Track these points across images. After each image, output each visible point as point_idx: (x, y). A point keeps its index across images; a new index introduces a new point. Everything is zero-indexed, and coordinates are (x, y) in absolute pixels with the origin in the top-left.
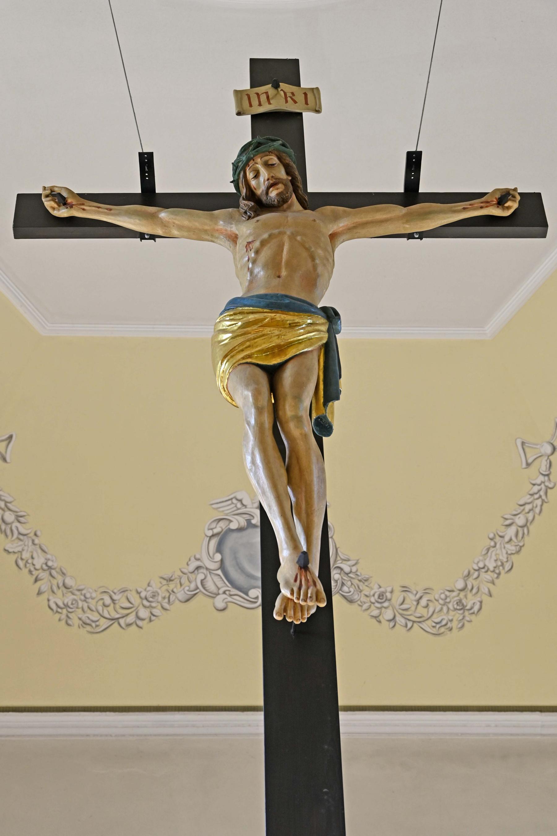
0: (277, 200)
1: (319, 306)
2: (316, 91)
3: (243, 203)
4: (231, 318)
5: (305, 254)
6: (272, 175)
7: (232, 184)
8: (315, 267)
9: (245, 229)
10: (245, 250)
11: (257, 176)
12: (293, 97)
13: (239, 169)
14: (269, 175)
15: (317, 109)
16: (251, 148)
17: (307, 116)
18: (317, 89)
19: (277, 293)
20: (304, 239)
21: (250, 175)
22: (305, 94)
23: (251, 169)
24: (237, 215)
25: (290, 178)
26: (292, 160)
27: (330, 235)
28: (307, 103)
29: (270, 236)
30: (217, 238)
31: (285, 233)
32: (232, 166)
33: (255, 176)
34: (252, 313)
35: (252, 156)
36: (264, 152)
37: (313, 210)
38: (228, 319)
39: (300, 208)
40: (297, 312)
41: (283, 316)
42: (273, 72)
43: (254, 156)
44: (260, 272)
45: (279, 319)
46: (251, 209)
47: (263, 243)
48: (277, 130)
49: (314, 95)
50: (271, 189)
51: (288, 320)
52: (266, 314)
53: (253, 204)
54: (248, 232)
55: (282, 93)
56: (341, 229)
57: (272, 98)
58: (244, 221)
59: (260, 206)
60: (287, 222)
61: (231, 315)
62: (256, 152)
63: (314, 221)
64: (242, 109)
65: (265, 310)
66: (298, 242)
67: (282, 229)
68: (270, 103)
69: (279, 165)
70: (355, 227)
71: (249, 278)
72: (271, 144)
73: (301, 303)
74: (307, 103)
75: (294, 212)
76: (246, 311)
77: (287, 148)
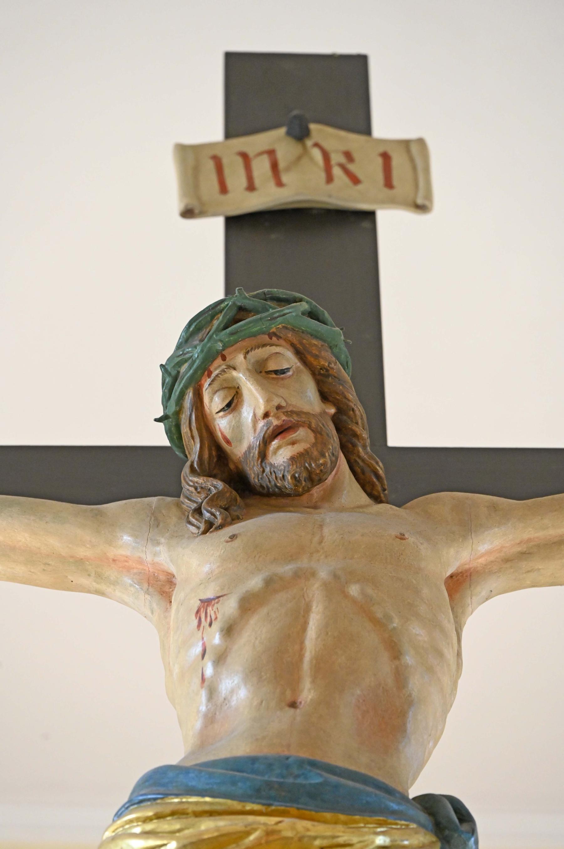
0: (293, 477)
1: (413, 793)
2: (415, 151)
3: (190, 482)
4: (149, 827)
5: (371, 638)
6: (277, 401)
7: (161, 425)
8: (400, 678)
9: (198, 562)
10: (196, 622)
11: (232, 404)
12: (351, 167)
13: (183, 381)
14: (268, 401)
15: (420, 201)
16: (216, 323)
17: (393, 226)
18: (421, 142)
19: (286, 753)
20: (370, 591)
21: (214, 402)
22: (386, 157)
23: (216, 385)
24: (173, 518)
25: (332, 411)
26: (338, 358)
27: (451, 576)
28: (389, 183)
29: (269, 582)
30: (115, 583)
31: (313, 574)
32: (159, 374)
33: (229, 405)
34: (211, 814)
35: (219, 346)
36: (254, 335)
37: (399, 505)
38: (138, 830)
39: (364, 498)
40: (344, 811)
41: (302, 825)
42: (293, 95)
43: (225, 347)
44: (237, 689)
45: (289, 834)
46: (213, 500)
47: (249, 604)
48: (300, 255)
49: (412, 160)
50: (275, 443)
51: (315, 838)
52: (251, 818)
53: (220, 485)
54: (206, 568)
55: (317, 154)
56: (482, 561)
57: (288, 169)
58: (194, 536)
59: (240, 490)
60: (321, 542)
61: (146, 820)
62: (232, 334)
63: (402, 537)
64: (199, 199)
65: (249, 807)
66: (354, 601)
67: (304, 563)
68: (279, 184)
69: (298, 371)
70: (524, 555)
71: (203, 708)
72: (275, 310)
73: (358, 786)
74: (389, 183)
75: (342, 509)
76: (191, 809)
77: (324, 323)
